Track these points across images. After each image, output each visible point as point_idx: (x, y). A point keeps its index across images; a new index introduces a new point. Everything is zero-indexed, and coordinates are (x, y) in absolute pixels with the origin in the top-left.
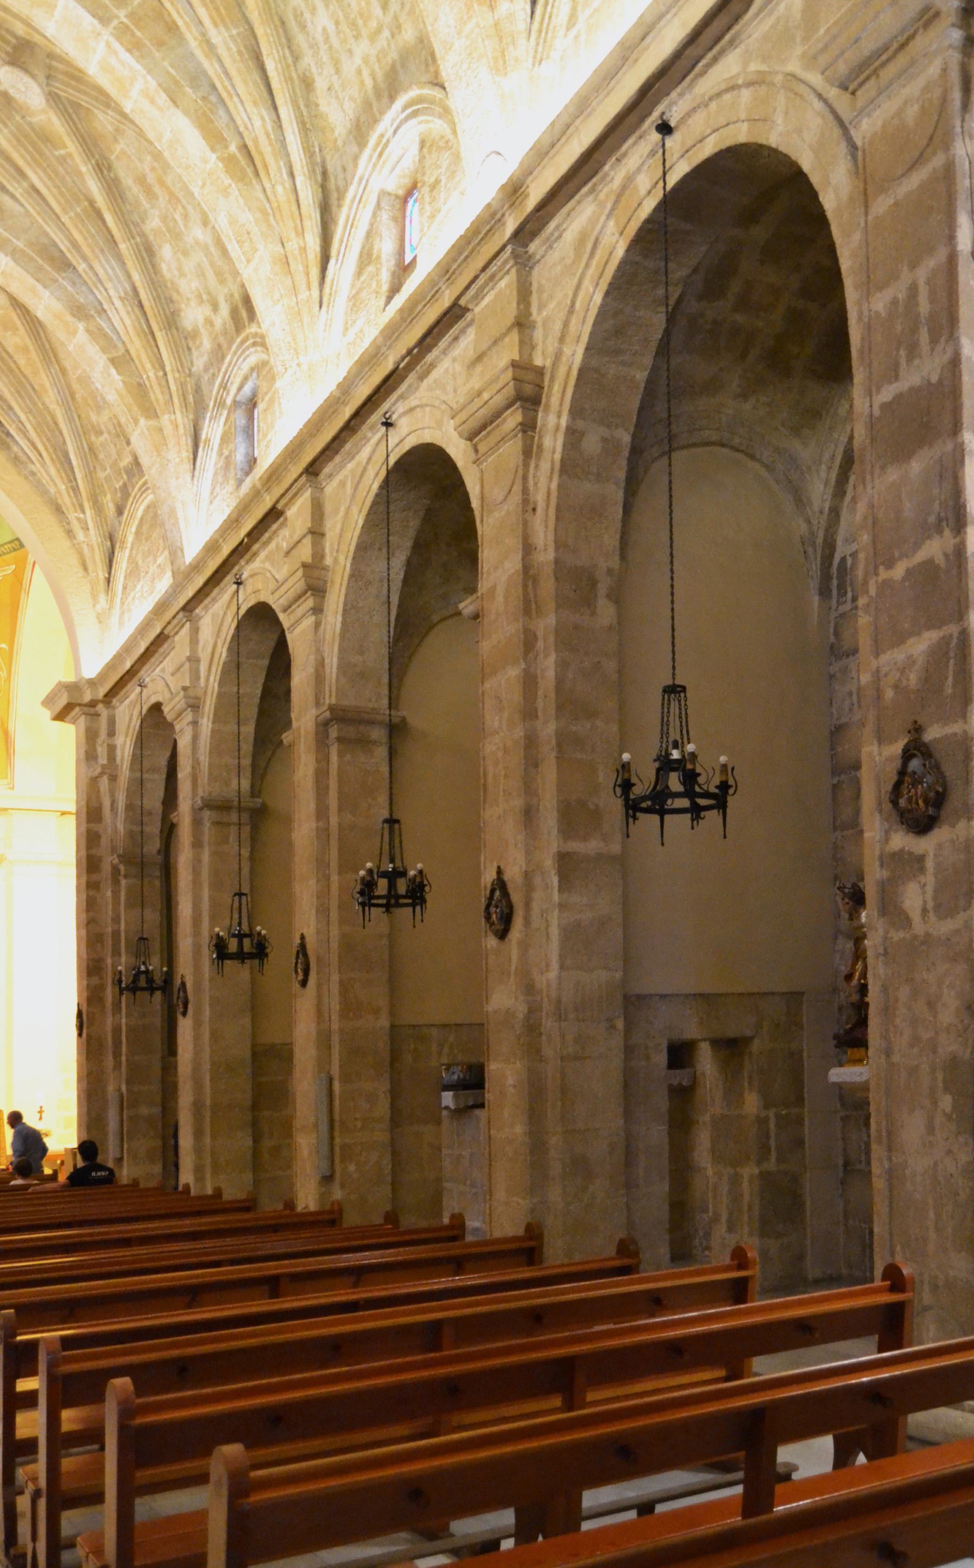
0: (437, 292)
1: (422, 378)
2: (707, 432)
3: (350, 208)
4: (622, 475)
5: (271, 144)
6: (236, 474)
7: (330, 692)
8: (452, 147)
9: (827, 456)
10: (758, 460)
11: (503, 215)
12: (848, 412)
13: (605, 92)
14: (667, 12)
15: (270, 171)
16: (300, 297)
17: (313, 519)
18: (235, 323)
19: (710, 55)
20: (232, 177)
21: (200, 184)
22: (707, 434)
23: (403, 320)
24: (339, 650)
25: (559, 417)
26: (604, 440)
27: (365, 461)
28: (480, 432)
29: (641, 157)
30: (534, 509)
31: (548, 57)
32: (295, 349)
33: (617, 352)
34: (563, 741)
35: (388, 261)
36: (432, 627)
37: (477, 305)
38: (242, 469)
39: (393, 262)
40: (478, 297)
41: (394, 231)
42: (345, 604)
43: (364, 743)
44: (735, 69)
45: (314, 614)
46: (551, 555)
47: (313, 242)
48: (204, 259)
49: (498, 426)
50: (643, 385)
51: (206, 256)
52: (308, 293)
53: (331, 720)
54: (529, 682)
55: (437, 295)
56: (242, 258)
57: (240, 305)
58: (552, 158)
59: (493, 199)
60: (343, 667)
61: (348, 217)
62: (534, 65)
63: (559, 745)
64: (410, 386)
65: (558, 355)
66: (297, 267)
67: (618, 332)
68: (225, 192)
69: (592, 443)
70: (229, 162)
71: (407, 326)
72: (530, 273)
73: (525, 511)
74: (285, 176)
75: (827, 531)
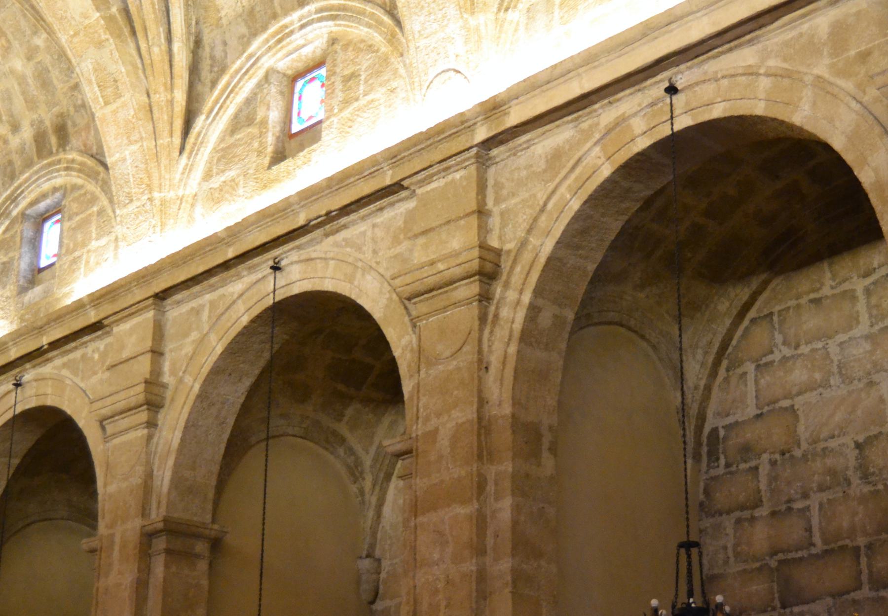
0: (377, 170)
1: (327, 235)
2: (612, 313)
3: (232, 77)
4: (563, 346)
5: (154, 13)
6: (18, 281)
7: (159, 503)
8: (377, 51)
9: (704, 342)
10: (647, 341)
11: (475, 124)
12: (728, 309)
13: (617, 54)
14: (698, 12)
15: (149, 34)
16: (160, 142)
17: (154, 339)
18: (37, 147)
19: (727, 46)
20: (111, 34)
21: (72, 33)
22: (611, 316)
23: (329, 187)
24: (175, 465)
25: (521, 292)
26: (555, 316)
27: (236, 296)
28: (423, 294)
29: (639, 105)
30: (487, 368)
31: (515, 7)
32: (148, 186)
33: (578, 247)
34: (519, 578)
35: (274, 127)
36: (251, 447)
37: (420, 187)
38: (25, 277)
39: (278, 129)
40: (428, 180)
41: (281, 103)
42: (188, 421)
43: (190, 556)
44: (751, 61)
45: (147, 427)
46: (507, 410)
47: (180, 96)
48: (16, 87)
49: (446, 292)
50: (591, 274)
51: (19, 84)
52: (169, 139)
53: (161, 531)
54: (481, 522)
55: (376, 173)
56: (101, 99)
57: (50, 131)
58: (543, 91)
59: (469, 111)
60: (177, 481)
61: (228, 84)
62: (499, 10)
63: (514, 582)
64: (312, 240)
65: (524, 243)
66: (161, 117)
67: (584, 232)
68: (100, 45)
69: (545, 319)
70: (110, 20)
71: (330, 193)
72: (486, 171)
73: (480, 369)
74: (163, 40)
75: (701, 404)
